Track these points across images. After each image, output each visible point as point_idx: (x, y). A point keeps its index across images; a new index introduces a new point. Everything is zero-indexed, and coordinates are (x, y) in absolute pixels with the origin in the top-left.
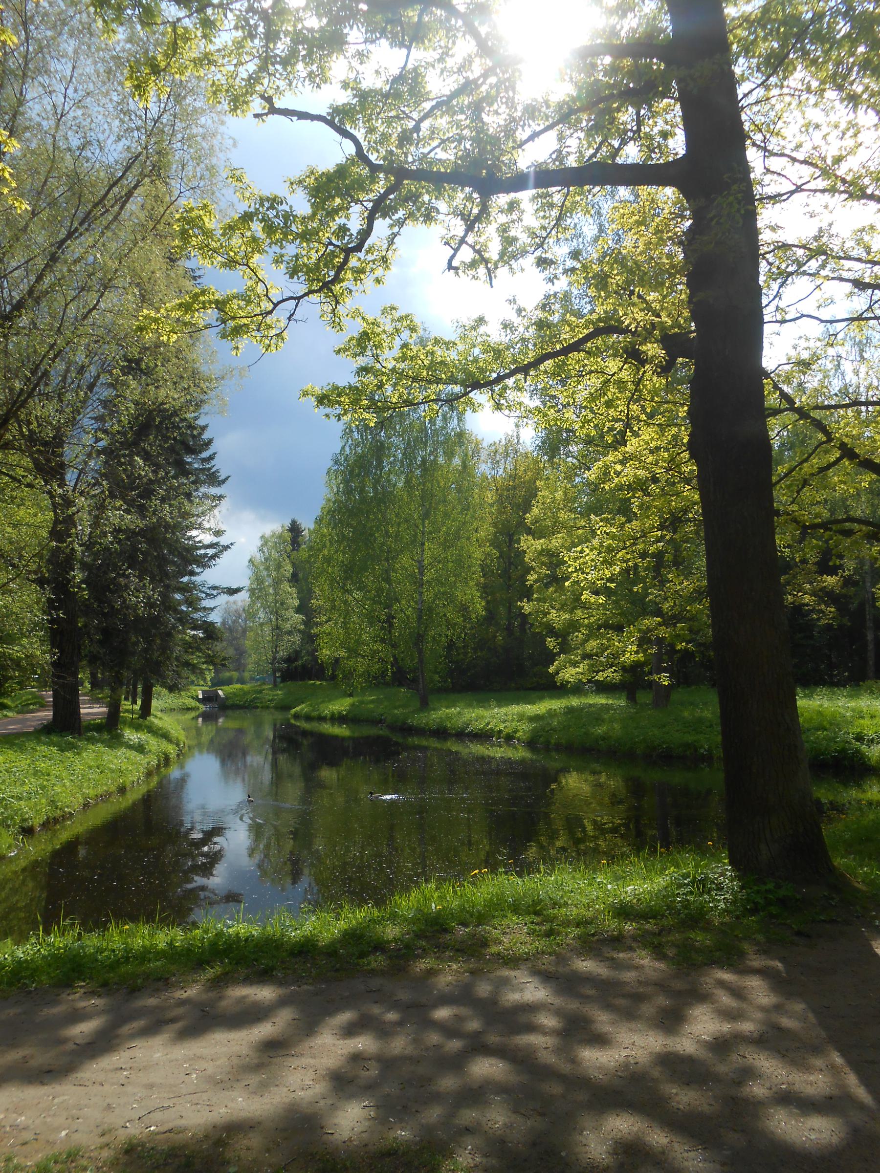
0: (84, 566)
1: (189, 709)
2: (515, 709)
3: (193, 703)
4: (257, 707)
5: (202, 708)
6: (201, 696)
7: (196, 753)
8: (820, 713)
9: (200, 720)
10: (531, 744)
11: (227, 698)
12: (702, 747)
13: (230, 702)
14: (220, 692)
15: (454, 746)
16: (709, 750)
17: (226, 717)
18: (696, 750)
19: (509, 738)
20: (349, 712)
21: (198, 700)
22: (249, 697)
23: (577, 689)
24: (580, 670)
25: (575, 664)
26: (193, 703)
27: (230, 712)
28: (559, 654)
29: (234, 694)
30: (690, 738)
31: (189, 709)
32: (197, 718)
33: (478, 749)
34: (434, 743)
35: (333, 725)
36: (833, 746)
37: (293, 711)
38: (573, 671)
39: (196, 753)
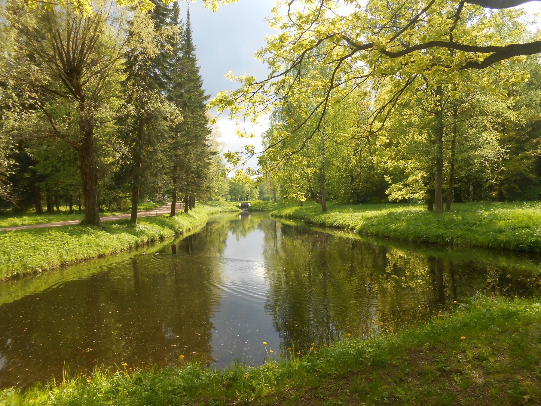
0: (37, 137)
1: (234, 211)
2: (359, 214)
3: (236, 209)
4: (265, 211)
5: (241, 211)
6: (240, 205)
7: (252, 231)
8: (530, 217)
9: (240, 216)
10: (360, 233)
11: (252, 206)
12: (447, 237)
13: (253, 208)
14: (249, 204)
15: (328, 231)
16: (452, 240)
17: (252, 215)
18: (443, 239)
19: (352, 229)
20: (294, 214)
21: (239, 207)
22: (262, 206)
23: (404, 202)
24: (403, 193)
25: (400, 190)
26: (236, 209)
27: (253, 213)
28: (391, 184)
29: (255, 204)
30: (440, 232)
31: (234, 211)
32: (239, 215)
33: (338, 234)
34: (319, 230)
35: (286, 220)
36: (530, 239)
37: (271, 213)
38: (400, 193)
39: (252, 231)
